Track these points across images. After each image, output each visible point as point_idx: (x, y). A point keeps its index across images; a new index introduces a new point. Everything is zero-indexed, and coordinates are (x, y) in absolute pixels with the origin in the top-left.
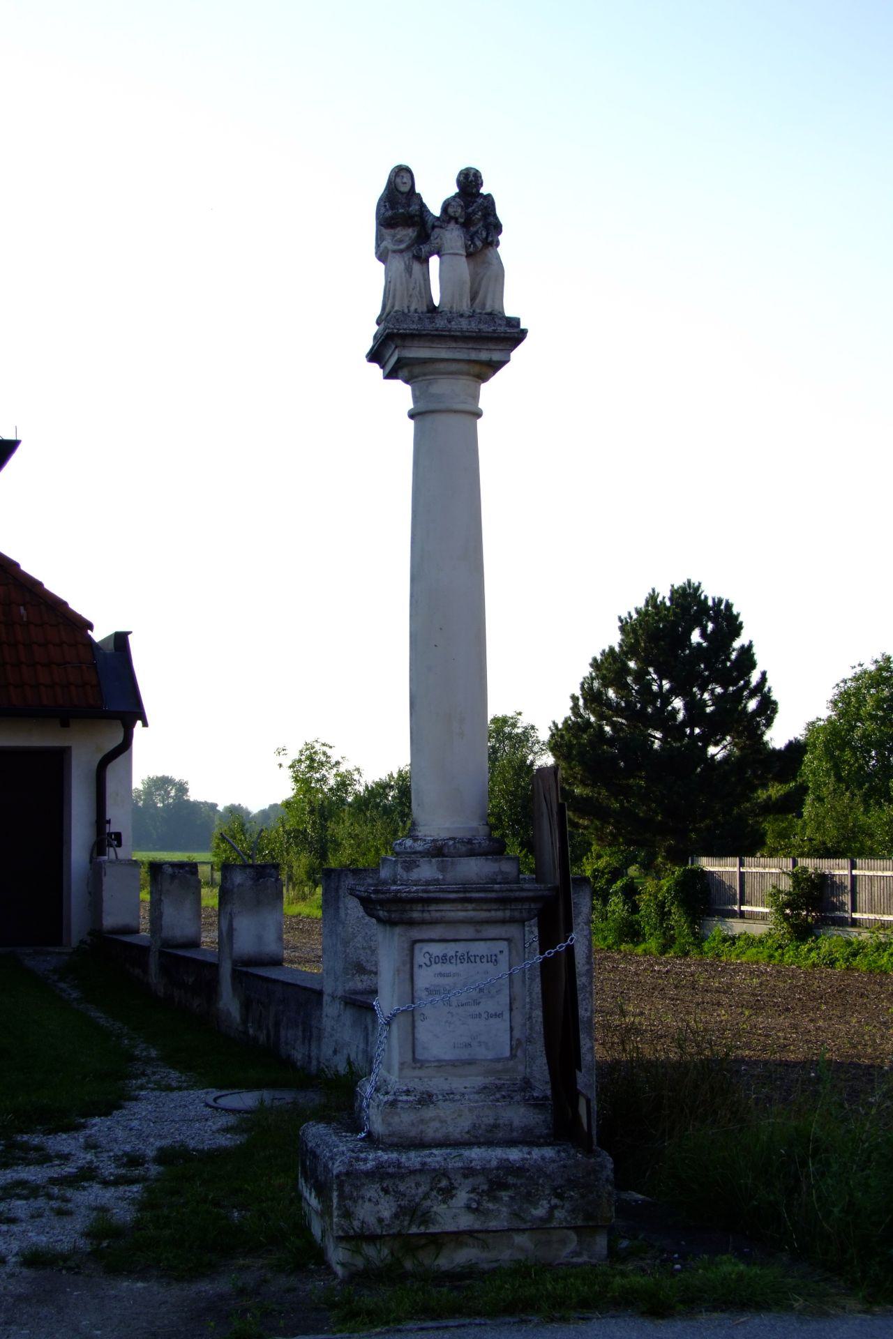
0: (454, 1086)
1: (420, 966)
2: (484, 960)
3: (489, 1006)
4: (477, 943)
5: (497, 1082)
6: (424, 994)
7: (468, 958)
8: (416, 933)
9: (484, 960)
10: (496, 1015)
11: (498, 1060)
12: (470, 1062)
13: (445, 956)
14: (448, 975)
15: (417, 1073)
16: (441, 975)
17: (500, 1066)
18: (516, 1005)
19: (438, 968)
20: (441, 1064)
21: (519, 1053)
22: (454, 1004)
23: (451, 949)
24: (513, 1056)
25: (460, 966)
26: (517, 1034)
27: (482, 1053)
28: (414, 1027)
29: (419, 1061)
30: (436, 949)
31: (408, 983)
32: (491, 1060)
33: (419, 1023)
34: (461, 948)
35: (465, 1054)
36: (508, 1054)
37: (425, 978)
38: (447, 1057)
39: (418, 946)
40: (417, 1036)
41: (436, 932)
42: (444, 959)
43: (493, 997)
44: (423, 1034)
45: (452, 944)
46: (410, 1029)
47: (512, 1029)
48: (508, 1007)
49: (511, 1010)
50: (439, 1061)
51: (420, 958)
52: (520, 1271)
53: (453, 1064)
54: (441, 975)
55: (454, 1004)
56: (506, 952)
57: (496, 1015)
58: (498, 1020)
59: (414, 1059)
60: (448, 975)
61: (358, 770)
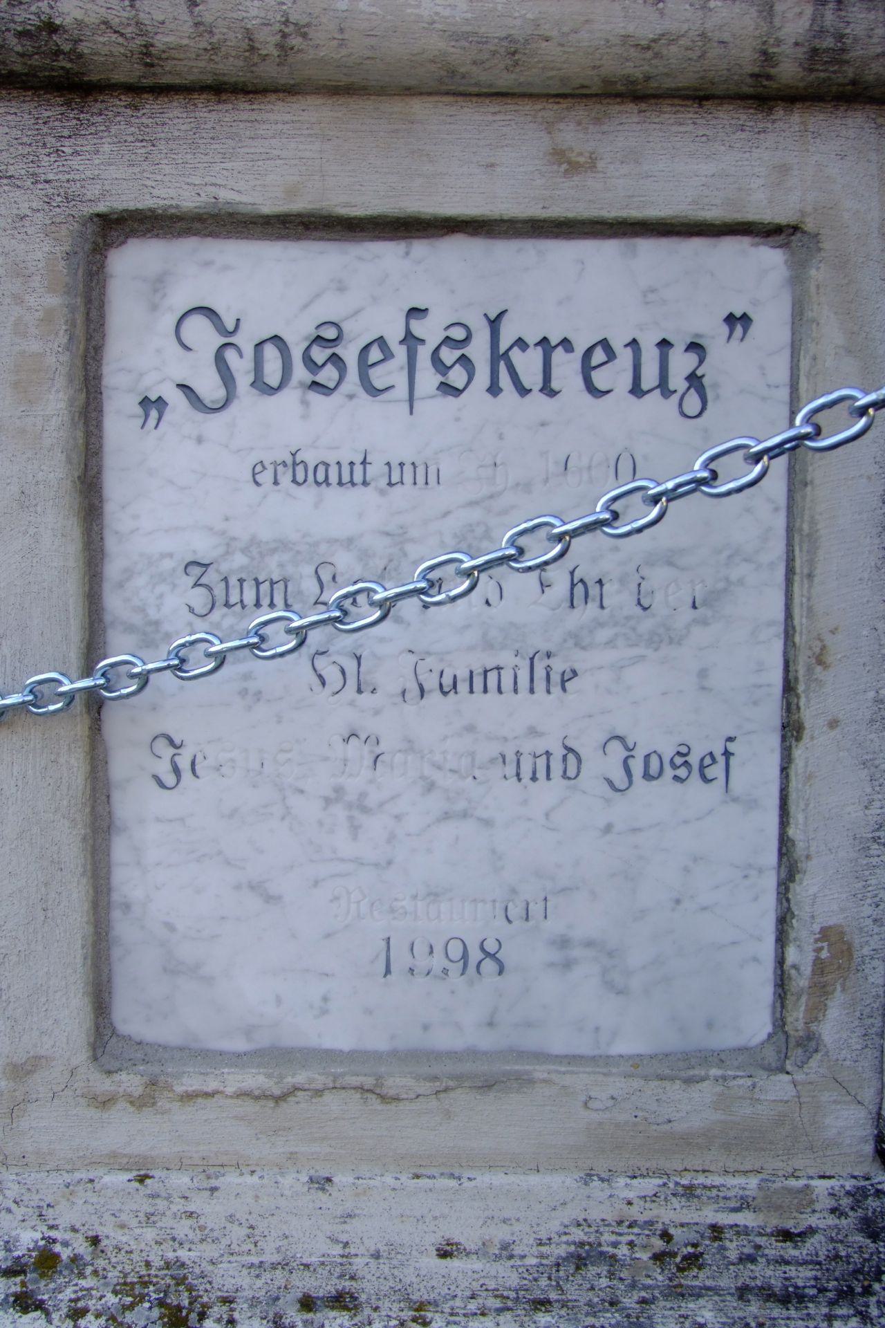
0: (368, 1232)
1: (152, 405)
2: (615, 376)
3: (643, 698)
4: (564, 254)
5: (672, 1213)
6: (175, 608)
7: (490, 359)
8: (120, 162)
9: (615, 376)
10: (685, 765)
11: (682, 1066)
12: (493, 1075)
13: (327, 339)
14: (351, 475)
15: (127, 1131)
16: (299, 471)
17: (692, 1107)
18: (832, 698)
19: (286, 421)
20: (287, 1077)
21: (836, 1026)
22: (392, 674)
23: (370, 289)
24: (790, 1044)
25: (435, 408)
26: (824, 897)
27: (570, 1011)
28: (99, 825)
29: (146, 1053)
30: (271, 288)
31: (55, 530)
32: (636, 1065)
33: (140, 803)
34: (451, 282)
35: (459, 1018)
36: (756, 1024)
37: (183, 491)
38: (337, 1035)
39: (132, 261)
40: (128, 881)
41: (264, 159)
42: (324, 360)
43: (664, 638)
44: (171, 862)
45: (387, 255)
46: (68, 843)
47: (789, 864)
48: (771, 710)
49: (791, 730)
50: (277, 1056)
51: (145, 352)
52: (794, 628)
53: (370, 1078)
54: (299, 471)
55: (392, 674)
56: (773, 324)
57: (685, 765)
58: (697, 794)
59: (103, 1033)
60: (351, 475)
61: (600, 582)
